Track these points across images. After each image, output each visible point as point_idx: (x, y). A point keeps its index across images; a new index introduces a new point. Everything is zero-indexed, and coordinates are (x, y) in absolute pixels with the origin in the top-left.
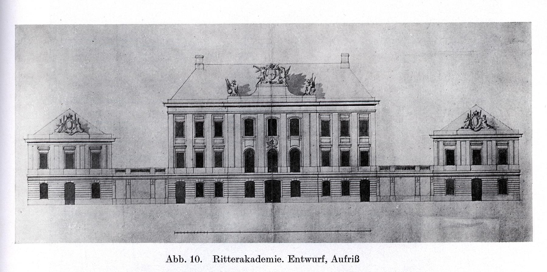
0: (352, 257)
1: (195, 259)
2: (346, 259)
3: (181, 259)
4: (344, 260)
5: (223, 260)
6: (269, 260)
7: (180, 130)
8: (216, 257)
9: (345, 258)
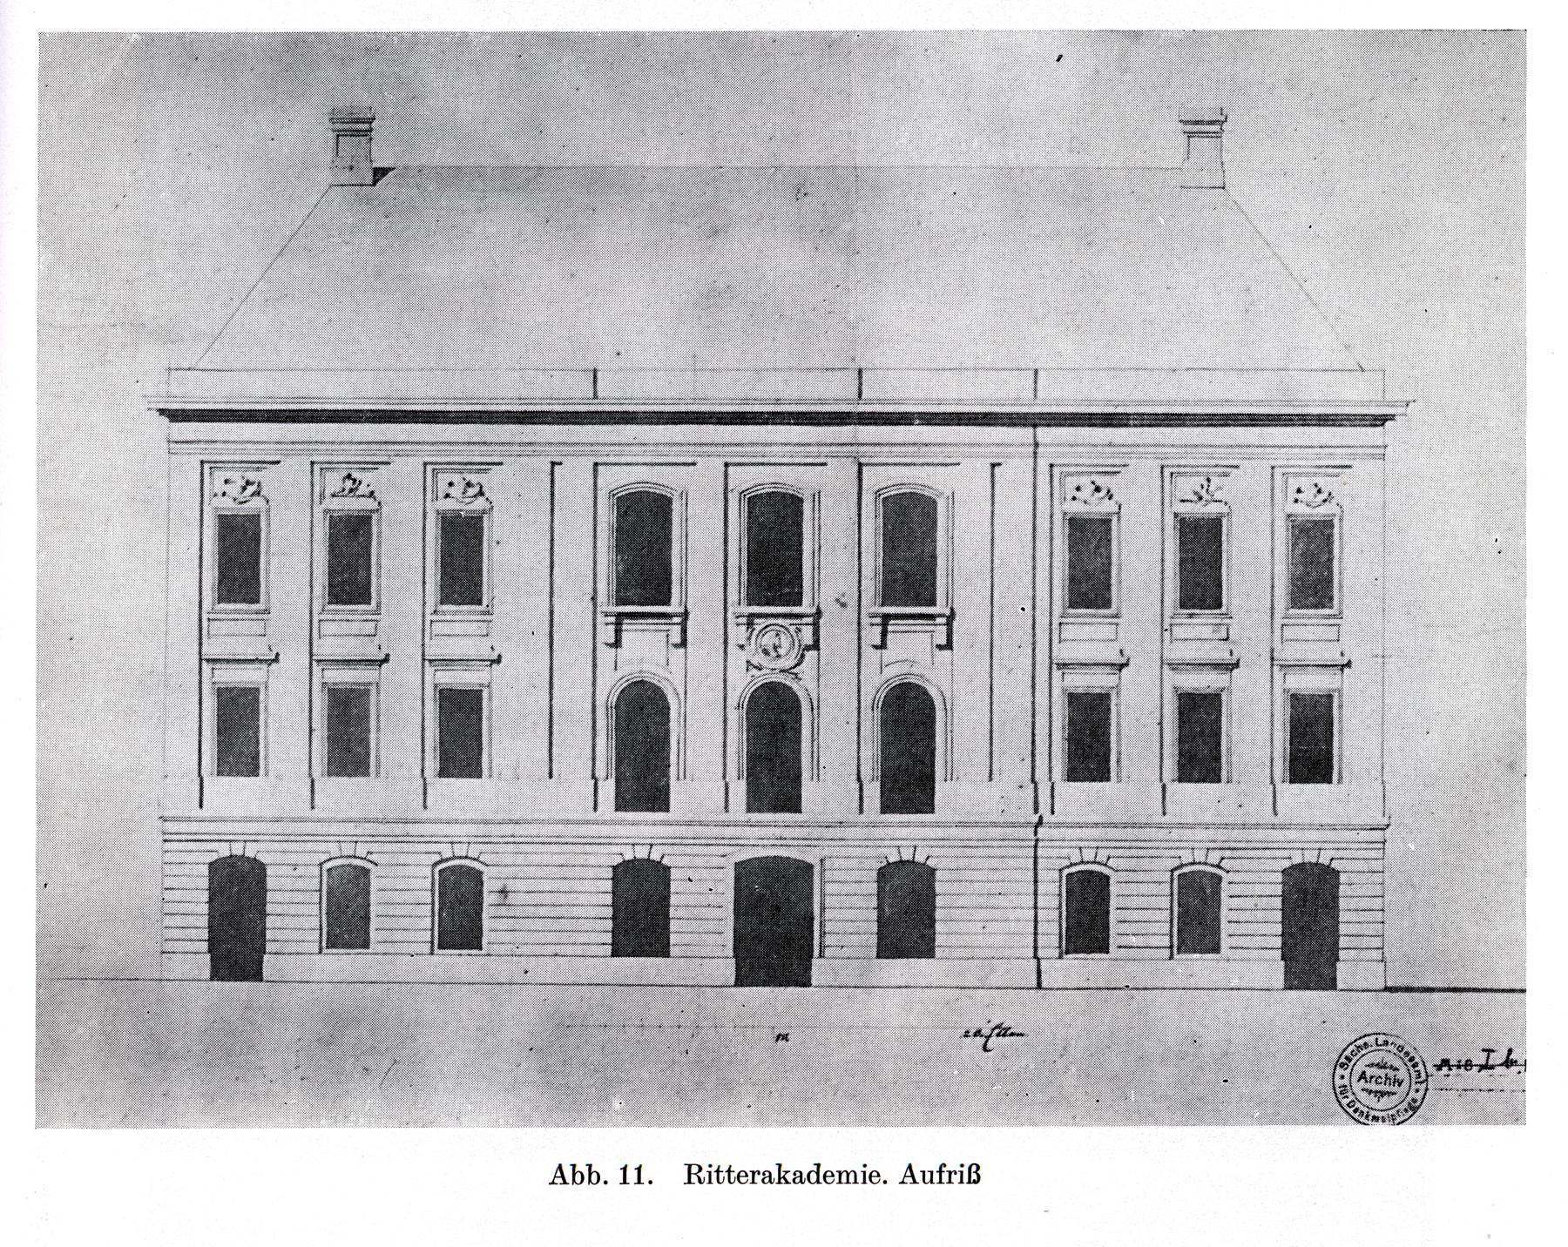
0: (959, 1169)
1: (632, 1175)
2: (942, 1174)
3: (592, 1175)
4: (936, 1178)
5: (714, 1175)
6: (845, 1177)
7: (238, 563)
8: (695, 1169)
9: (940, 1172)
